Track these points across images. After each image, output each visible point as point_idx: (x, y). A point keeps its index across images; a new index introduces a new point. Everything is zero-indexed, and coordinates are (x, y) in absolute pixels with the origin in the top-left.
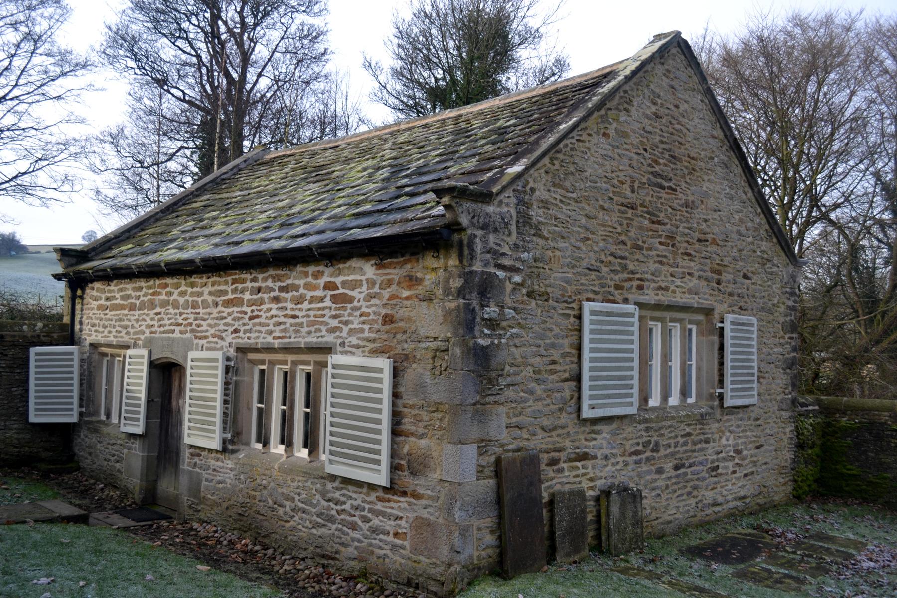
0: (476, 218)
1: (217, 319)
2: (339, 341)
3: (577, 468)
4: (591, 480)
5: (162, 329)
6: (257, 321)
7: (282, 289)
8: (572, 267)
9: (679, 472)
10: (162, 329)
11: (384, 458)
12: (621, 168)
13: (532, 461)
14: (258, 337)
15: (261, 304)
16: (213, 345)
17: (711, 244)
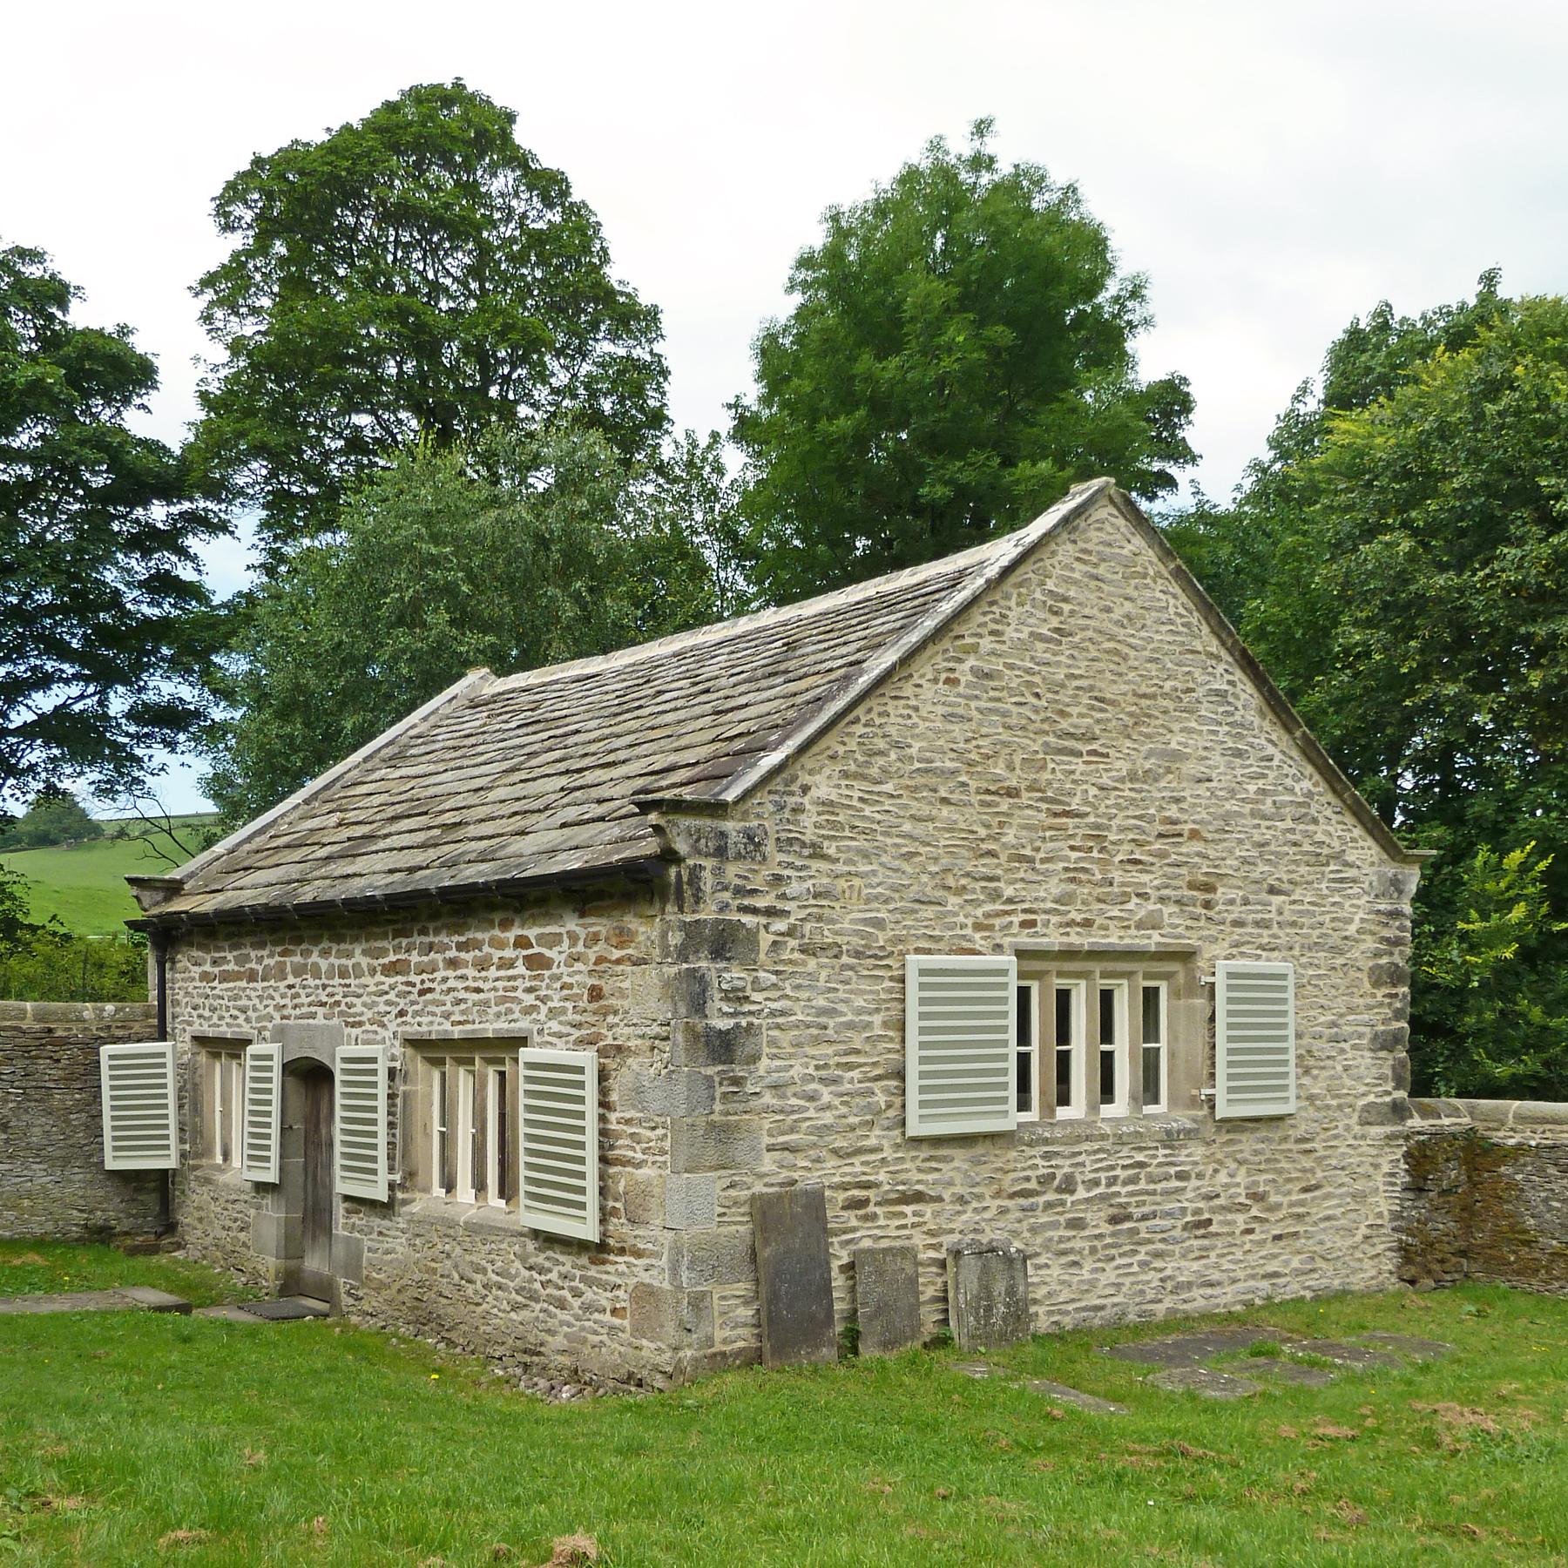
0: (703, 841)
1: (374, 994)
2: (536, 1028)
3: (903, 1215)
4: (930, 1233)
5: (298, 1012)
6: (429, 996)
7: (461, 947)
8: (886, 902)
9: (1119, 1227)
10: (298, 1012)
11: (591, 1198)
12: (984, 731)
13: (815, 1202)
14: (431, 1023)
15: (434, 971)
16: (371, 1036)
17: (1190, 838)
